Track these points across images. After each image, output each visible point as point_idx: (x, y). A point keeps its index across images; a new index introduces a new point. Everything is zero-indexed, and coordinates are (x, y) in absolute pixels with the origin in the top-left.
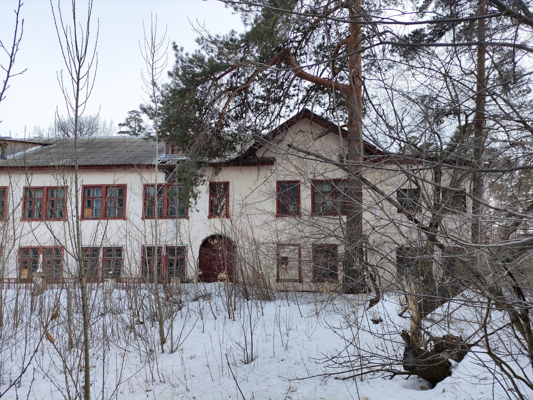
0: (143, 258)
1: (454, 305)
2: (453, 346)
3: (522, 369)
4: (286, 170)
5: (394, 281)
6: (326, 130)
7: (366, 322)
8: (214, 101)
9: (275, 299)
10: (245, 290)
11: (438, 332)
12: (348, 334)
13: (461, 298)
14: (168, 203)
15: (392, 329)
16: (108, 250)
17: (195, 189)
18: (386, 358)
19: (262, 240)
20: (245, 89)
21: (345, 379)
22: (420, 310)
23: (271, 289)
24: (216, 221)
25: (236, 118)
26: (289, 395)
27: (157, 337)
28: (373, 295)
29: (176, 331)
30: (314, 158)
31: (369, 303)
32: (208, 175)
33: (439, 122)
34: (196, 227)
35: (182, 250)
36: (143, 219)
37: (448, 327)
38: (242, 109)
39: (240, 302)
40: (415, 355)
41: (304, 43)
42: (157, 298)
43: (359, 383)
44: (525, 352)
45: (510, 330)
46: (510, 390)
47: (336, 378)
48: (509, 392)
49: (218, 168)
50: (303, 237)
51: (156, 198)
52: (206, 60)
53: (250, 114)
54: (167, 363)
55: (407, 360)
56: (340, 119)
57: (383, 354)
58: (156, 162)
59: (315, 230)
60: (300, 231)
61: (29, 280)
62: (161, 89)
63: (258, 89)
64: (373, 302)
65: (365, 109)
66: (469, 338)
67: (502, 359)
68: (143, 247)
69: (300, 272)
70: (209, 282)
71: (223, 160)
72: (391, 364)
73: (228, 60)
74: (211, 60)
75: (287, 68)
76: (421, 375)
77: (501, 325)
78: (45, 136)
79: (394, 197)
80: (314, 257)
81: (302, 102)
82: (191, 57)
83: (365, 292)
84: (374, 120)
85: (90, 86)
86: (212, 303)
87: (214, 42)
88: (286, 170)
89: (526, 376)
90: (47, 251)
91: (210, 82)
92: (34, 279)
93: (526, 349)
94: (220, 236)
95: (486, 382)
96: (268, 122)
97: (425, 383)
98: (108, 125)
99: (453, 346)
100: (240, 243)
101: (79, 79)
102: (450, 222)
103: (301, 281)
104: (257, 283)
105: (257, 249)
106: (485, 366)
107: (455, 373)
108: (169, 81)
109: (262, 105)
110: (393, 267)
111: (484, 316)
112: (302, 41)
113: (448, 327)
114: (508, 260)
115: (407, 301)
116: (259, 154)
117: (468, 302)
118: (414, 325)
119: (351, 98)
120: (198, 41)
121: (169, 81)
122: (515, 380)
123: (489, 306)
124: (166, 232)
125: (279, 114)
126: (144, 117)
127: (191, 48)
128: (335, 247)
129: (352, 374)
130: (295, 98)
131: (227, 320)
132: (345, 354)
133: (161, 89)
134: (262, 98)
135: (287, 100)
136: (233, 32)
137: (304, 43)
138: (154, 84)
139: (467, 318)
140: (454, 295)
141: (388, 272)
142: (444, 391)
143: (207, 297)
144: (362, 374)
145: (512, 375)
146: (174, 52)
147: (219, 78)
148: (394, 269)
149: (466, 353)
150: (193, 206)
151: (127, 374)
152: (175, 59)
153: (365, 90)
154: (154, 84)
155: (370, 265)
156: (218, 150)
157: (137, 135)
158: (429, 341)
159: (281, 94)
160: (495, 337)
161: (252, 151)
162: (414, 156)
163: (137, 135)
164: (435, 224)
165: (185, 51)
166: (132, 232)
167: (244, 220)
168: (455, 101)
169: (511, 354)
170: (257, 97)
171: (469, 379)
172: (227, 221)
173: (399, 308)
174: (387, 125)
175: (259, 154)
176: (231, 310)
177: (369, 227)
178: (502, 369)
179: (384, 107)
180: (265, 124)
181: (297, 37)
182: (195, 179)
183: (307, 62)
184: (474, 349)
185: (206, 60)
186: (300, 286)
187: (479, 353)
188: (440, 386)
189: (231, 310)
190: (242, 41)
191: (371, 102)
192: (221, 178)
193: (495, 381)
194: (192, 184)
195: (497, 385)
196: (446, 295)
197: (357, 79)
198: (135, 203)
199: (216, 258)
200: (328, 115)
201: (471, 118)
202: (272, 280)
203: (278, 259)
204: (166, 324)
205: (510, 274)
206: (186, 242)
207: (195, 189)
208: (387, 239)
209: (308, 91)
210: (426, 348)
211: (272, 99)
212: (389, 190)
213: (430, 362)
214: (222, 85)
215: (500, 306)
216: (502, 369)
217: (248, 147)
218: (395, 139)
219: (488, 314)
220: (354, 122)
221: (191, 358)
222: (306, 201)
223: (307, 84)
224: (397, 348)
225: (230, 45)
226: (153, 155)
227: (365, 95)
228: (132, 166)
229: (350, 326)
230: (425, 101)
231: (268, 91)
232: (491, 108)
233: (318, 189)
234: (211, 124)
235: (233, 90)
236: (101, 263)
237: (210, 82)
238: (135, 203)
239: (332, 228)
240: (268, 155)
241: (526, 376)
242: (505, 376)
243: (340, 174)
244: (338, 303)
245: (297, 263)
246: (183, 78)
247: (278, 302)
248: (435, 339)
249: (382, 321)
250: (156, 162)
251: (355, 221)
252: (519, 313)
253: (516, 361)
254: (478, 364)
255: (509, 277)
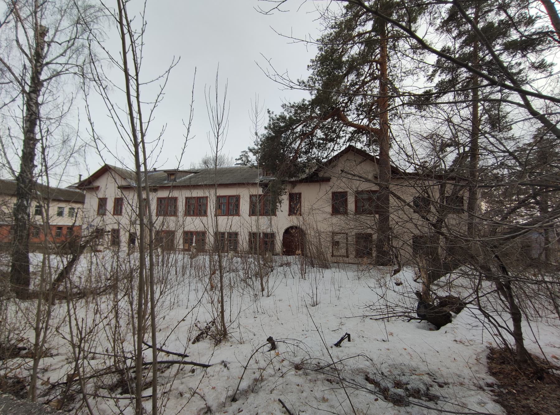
0: (249, 239)
1: (453, 276)
2: (453, 304)
3: (505, 322)
4: (339, 184)
5: (411, 258)
6: (365, 158)
7: (391, 284)
8: (292, 142)
9: (331, 268)
10: (312, 261)
11: (442, 293)
12: (380, 291)
13: (460, 272)
14: (264, 207)
15: (409, 290)
16: (229, 234)
17: (280, 198)
18: (406, 308)
19: (322, 230)
20: (312, 134)
21: (376, 319)
22: (429, 278)
23: (328, 261)
24: (294, 218)
25: (306, 153)
26: (340, 327)
27: (260, 287)
28: (396, 267)
29: (271, 283)
30: (358, 178)
31: (393, 272)
32: (288, 189)
33: (442, 150)
34: (281, 221)
35: (273, 235)
36: (250, 216)
37: (450, 290)
38: (309, 147)
39: (308, 269)
40: (426, 307)
41: (349, 104)
42: (259, 264)
43: (386, 323)
44: (508, 310)
45: (496, 295)
46: (496, 335)
47: (371, 319)
48: (495, 337)
49: (294, 184)
50: (349, 229)
51: (258, 204)
52: (287, 118)
53: (315, 150)
54: (265, 302)
55: (421, 310)
56: (374, 151)
57: (403, 305)
58: (257, 181)
59: (357, 224)
60: (347, 224)
61: (189, 250)
62: (260, 137)
63: (319, 134)
64: (396, 272)
65: (390, 144)
66: (465, 298)
67: (490, 314)
68: (250, 233)
69: (347, 251)
70: (289, 255)
71: (297, 179)
72: (409, 312)
73: (300, 117)
74: (290, 118)
75: (338, 120)
76: (430, 320)
77: (489, 291)
78: (196, 168)
79: (412, 204)
80: (356, 242)
81: (348, 141)
82: (278, 117)
83: (391, 265)
84: (397, 151)
85: (224, 139)
86: (291, 269)
87: (293, 107)
88: (339, 184)
89: (508, 327)
90: (197, 233)
91: (290, 131)
92: (192, 249)
93: (508, 308)
94: (296, 227)
95: (477, 328)
96: (326, 154)
97: (432, 326)
98: (230, 160)
99: (453, 304)
100: (309, 231)
101: (218, 136)
102: (452, 219)
103: (348, 257)
104: (319, 257)
105: (319, 235)
106: (476, 318)
107: (454, 321)
108: (265, 132)
109: (322, 144)
110: (409, 248)
111: (477, 284)
112: (348, 102)
113: (450, 290)
114: (495, 247)
115: (420, 271)
116: (321, 174)
117: (464, 274)
118: (425, 288)
119: (382, 137)
120: (283, 106)
121: (265, 132)
122: (499, 328)
123: (480, 278)
124: (263, 224)
125: (333, 149)
126: (250, 154)
127: (278, 111)
128: (370, 235)
129: (382, 317)
130: (344, 139)
131: (301, 279)
132: (377, 304)
133: (260, 137)
134: (322, 139)
135: (338, 140)
136: (304, 100)
137: (349, 104)
138: (256, 134)
139: (464, 285)
140: (454, 269)
141: (407, 252)
142: (446, 332)
143: (288, 264)
144: (388, 317)
145: (497, 325)
146: (268, 115)
147: (295, 128)
148: (410, 250)
149: (463, 308)
150: (279, 208)
151: (244, 308)
152: (269, 119)
153: (391, 132)
154: (256, 134)
155: (394, 247)
156: (295, 173)
157: (246, 165)
158: (436, 298)
159: (334, 136)
160: (484, 299)
161: (315, 174)
162: (425, 173)
163: (246, 165)
164: (440, 221)
165: (275, 113)
166: (243, 224)
167: (311, 217)
168: (455, 136)
169: (497, 311)
170: (319, 139)
171: (465, 326)
172: (301, 218)
173: (414, 276)
174: (407, 155)
175: (321, 174)
176: (303, 273)
177: (394, 222)
178: (490, 321)
179: (404, 143)
180: (324, 155)
181: (344, 100)
182: (280, 192)
183: (351, 117)
184: (468, 306)
185: (287, 118)
186: (346, 259)
187: (473, 309)
188: (443, 329)
189: (303, 273)
190: (309, 105)
191: (395, 139)
192: (296, 190)
193: (484, 328)
194: (279, 195)
195: (485, 330)
196: (448, 269)
197: (385, 125)
198: (245, 206)
199: (294, 241)
200: (366, 148)
201: (467, 149)
202: (329, 256)
203: (333, 243)
204: (265, 280)
205: (496, 256)
206: (275, 230)
207: (280, 198)
208: (405, 230)
209: (352, 134)
210: (433, 303)
211: (328, 139)
212: (409, 199)
213: (436, 312)
214: (297, 132)
215: (488, 278)
216: (490, 321)
217: (313, 170)
218: (412, 163)
219: (480, 283)
220: (384, 153)
221: (280, 301)
222: (351, 206)
223: (351, 129)
224: (413, 303)
225: (302, 108)
226: (256, 176)
227: (391, 135)
228: (243, 184)
229: (381, 287)
230: (432, 137)
231: (326, 135)
232: (481, 140)
233: (360, 197)
234: (290, 157)
235: (304, 135)
236: (227, 242)
237: (290, 131)
238: (245, 206)
239: (369, 223)
240: (327, 175)
241: (508, 327)
242: (492, 325)
243: (375, 188)
244: (374, 272)
245: (345, 245)
246: (274, 130)
247: (333, 269)
248: (440, 298)
249: (402, 284)
250: (257, 181)
251: (385, 219)
252: (503, 283)
253: (500, 316)
254: (472, 316)
255: (496, 259)
